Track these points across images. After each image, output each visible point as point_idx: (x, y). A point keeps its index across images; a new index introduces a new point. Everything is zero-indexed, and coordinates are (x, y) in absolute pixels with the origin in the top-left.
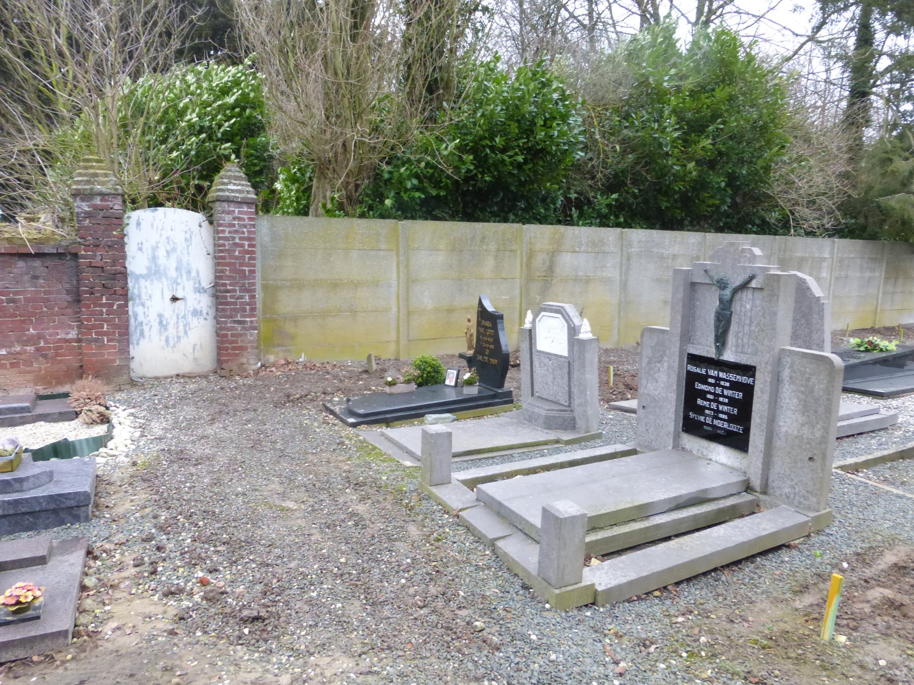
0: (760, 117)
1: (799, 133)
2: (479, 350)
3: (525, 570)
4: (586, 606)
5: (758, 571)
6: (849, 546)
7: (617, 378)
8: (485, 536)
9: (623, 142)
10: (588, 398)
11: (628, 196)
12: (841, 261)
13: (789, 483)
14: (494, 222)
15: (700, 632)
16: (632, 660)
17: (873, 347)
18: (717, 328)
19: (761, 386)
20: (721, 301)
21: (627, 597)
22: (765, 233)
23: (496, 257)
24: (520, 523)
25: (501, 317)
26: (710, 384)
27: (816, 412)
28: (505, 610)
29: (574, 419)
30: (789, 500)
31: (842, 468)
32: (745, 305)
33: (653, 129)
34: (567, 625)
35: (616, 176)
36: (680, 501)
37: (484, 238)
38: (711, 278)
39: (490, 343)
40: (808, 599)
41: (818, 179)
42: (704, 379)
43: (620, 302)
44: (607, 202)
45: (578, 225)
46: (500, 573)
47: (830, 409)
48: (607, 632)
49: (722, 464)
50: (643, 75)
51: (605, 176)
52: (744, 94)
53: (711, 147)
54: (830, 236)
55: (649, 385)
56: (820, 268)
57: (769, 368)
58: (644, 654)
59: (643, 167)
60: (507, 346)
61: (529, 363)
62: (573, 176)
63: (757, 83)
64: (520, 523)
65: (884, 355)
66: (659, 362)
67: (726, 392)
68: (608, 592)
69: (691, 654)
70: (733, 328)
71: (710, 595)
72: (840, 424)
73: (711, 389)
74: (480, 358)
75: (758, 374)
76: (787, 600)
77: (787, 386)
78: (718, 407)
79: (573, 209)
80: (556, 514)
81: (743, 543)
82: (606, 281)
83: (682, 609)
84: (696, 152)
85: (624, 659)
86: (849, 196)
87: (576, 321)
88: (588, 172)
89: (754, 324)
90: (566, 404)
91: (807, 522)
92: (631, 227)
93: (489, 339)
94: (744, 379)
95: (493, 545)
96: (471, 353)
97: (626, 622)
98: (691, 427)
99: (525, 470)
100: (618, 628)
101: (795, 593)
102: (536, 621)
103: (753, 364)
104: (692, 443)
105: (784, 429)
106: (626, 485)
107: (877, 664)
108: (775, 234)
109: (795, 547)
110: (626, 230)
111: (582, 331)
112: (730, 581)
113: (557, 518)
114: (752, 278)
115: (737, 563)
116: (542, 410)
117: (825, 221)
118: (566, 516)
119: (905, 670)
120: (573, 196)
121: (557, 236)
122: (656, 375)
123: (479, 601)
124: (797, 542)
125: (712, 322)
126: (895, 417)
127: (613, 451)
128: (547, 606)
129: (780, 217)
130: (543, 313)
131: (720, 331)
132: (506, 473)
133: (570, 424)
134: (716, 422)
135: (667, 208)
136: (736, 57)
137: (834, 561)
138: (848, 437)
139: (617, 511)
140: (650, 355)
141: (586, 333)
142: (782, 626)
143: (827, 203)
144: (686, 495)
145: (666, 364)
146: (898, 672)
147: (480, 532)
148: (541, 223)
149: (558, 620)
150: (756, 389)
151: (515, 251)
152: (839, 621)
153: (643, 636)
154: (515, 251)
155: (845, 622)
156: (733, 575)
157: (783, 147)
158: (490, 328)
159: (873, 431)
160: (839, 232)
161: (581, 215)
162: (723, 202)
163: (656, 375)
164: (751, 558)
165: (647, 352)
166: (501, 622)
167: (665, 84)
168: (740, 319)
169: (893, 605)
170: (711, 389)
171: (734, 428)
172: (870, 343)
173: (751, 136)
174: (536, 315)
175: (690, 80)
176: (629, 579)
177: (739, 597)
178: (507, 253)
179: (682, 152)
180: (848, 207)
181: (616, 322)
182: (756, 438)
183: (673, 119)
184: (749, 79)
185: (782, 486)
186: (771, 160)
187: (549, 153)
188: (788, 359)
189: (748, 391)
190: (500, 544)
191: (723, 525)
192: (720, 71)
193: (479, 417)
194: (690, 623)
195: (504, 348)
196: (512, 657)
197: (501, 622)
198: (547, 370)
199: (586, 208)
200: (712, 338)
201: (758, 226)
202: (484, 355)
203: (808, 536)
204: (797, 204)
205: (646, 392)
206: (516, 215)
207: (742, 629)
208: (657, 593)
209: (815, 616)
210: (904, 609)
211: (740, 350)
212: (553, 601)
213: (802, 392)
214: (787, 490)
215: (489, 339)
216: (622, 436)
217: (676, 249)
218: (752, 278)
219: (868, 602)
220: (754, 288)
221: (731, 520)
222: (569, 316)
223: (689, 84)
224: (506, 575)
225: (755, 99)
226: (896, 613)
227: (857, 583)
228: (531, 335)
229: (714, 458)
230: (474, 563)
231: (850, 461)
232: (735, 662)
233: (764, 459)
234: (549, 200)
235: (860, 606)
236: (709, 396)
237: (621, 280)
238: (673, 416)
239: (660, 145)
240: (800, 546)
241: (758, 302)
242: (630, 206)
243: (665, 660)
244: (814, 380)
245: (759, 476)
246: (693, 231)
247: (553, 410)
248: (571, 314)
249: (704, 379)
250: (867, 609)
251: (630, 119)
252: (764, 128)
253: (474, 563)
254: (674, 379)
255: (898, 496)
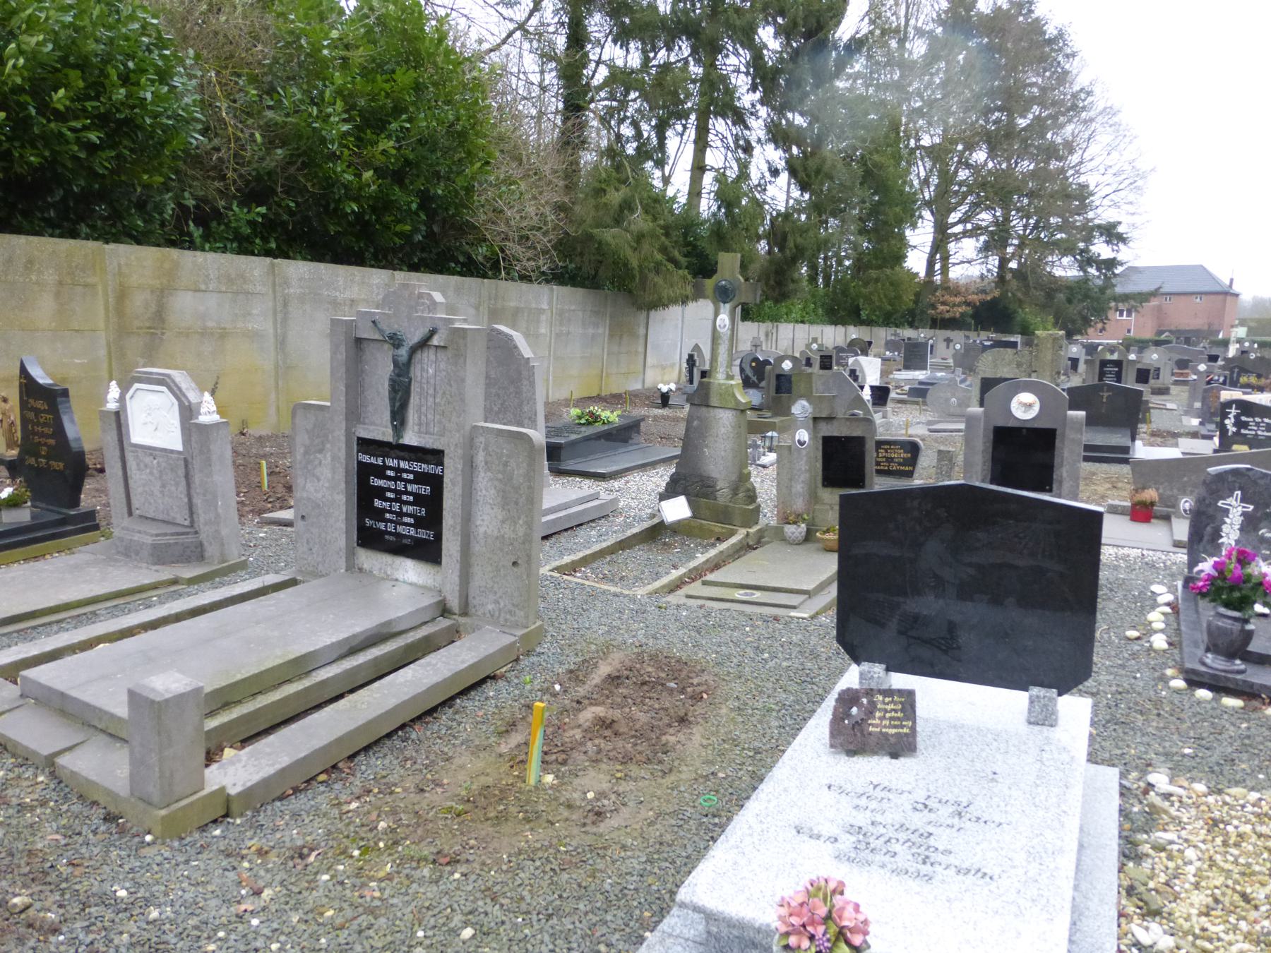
0: (458, 119)
1: (507, 147)
2: (28, 446)
3: (109, 793)
4: (215, 821)
5: (457, 717)
6: (561, 663)
7: (274, 478)
8: (34, 753)
9: (267, 128)
10: (220, 511)
11: (281, 211)
12: (561, 313)
13: (492, 597)
14: (52, 236)
15: (379, 816)
16: (281, 883)
17: (595, 418)
18: (392, 400)
19: (451, 476)
20: (395, 363)
21: (278, 793)
22: (472, 275)
23: (58, 295)
24: (100, 719)
25: (65, 393)
26: (389, 478)
27: (517, 503)
28: (71, 864)
29: (201, 544)
30: (493, 619)
31: (557, 569)
32: (427, 369)
33: (310, 115)
34: (181, 859)
35: (258, 178)
36: (356, 642)
37: (30, 262)
38: (381, 331)
39: (48, 436)
40: (516, 738)
41: (531, 210)
42: (380, 472)
43: (277, 367)
44: (249, 217)
45: (203, 250)
46: (65, 807)
47: (532, 500)
48: (244, 852)
49: (411, 584)
50: (291, 32)
51: (241, 176)
52: (435, 84)
53: (394, 152)
54: (547, 281)
55: (308, 485)
56: (538, 321)
57: (460, 451)
58: (299, 867)
59: (298, 169)
60: (78, 440)
61: (119, 465)
62: (190, 172)
63: (451, 72)
64: (100, 719)
65: (606, 427)
66: (321, 451)
67: (409, 487)
68: (249, 795)
69: (365, 850)
70: (414, 400)
71: (395, 762)
72: (544, 519)
73: (391, 484)
74: (32, 461)
75: (447, 461)
76: (491, 746)
77: (482, 474)
78: (401, 508)
79: (191, 224)
80: (152, 696)
81: (437, 684)
82: (254, 336)
83: (357, 791)
84: (374, 156)
85: (269, 885)
86: (567, 234)
87: (192, 396)
88: (214, 168)
89: (439, 396)
90: (187, 523)
91: (514, 643)
92: (288, 257)
93: (46, 430)
94: (426, 468)
95: (53, 764)
96: (13, 453)
97: (275, 829)
98: (369, 538)
99: (114, 633)
100: (264, 841)
101: (500, 734)
102: (127, 867)
103: (440, 448)
104: (371, 560)
105: (482, 530)
106: (276, 633)
107: (585, 799)
108: (484, 276)
109: (502, 676)
110: (278, 261)
111: (202, 410)
112: (422, 738)
113: (153, 702)
114: (433, 333)
115: (431, 712)
116: (146, 536)
117: (541, 262)
118: (167, 696)
119: (613, 797)
120: (191, 203)
121: (167, 265)
122: (317, 472)
123: (23, 862)
124: (503, 670)
125: (387, 394)
126: (616, 500)
127: (261, 585)
128: (148, 838)
129: (488, 254)
130: (136, 386)
131: (397, 404)
132: (80, 643)
133: (197, 553)
134: (400, 529)
135: (338, 233)
136: (422, 30)
137: (546, 685)
138: (566, 530)
139: (261, 673)
140: (307, 442)
141: (208, 413)
142: (484, 780)
143: (543, 241)
144: (362, 633)
145: (328, 455)
146: (606, 802)
147: (26, 748)
148: (139, 243)
149: (167, 854)
150: (446, 480)
151: (93, 286)
152: (547, 758)
153: (299, 843)
154: (93, 286)
155: (554, 757)
156: (426, 729)
157: (487, 163)
158: (44, 411)
159: (593, 521)
160: (559, 277)
161: (207, 237)
162: (416, 230)
163: (317, 472)
164: (448, 702)
165: (302, 439)
166: (64, 885)
167: (325, 52)
168: (422, 388)
169: (605, 724)
170: (391, 484)
171: (423, 534)
172: (591, 414)
173: (447, 144)
174: (124, 388)
175: (361, 51)
176: (278, 767)
177: (432, 757)
178: (79, 289)
179: (355, 153)
180: (565, 246)
181: (273, 396)
182: (451, 545)
183: (339, 105)
184: (440, 65)
185: (485, 603)
186: (473, 178)
187: (140, 127)
188: (482, 439)
189: (436, 483)
190: (62, 761)
191: (412, 666)
192: (403, 46)
193: (36, 558)
194: (367, 807)
195: (73, 445)
196: (81, 936)
197: (64, 885)
198: (151, 473)
199: (214, 224)
200: (387, 415)
201: (463, 265)
202: (37, 455)
203: (517, 660)
204: (507, 239)
205: (305, 495)
206: (93, 227)
207: (435, 798)
208: (323, 777)
209: (519, 760)
210: (615, 726)
211: (424, 429)
212: (158, 829)
213: (500, 480)
214: (490, 607)
215: (46, 430)
216: (277, 562)
217: (354, 292)
218: (433, 333)
219: (580, 726)
220: (437, 347)
221: (424, 655)
222: (180, 389)
223: (359, 55)
224: (76, 808)
225: (450, 92)
226: (608, 733)
227: (568, 707)
228: (119, 420)
229: (401, 577)
230: (14, 801)
231: (567, 559)
232: (424, 843)
233: (461, 571)
234: (149, 207)
235: (571, 733)
236: (390, 495)
237: (276, 336)
238: (343, 526)
239: (323, 141)
240: (508, 675)
241: (442, 366)
242: (284, 224)
243: (329, 869)
244: (513, 463)
245: (457, 594)
246: (379, 267)
247: (165, 535)
248: (184, 386)
249: (380, 472)
250: (578, 734)
251: (276, 96)
252: (462, 135)
253: (14, 801)
254: (341, 475)
255: (616, 595)
